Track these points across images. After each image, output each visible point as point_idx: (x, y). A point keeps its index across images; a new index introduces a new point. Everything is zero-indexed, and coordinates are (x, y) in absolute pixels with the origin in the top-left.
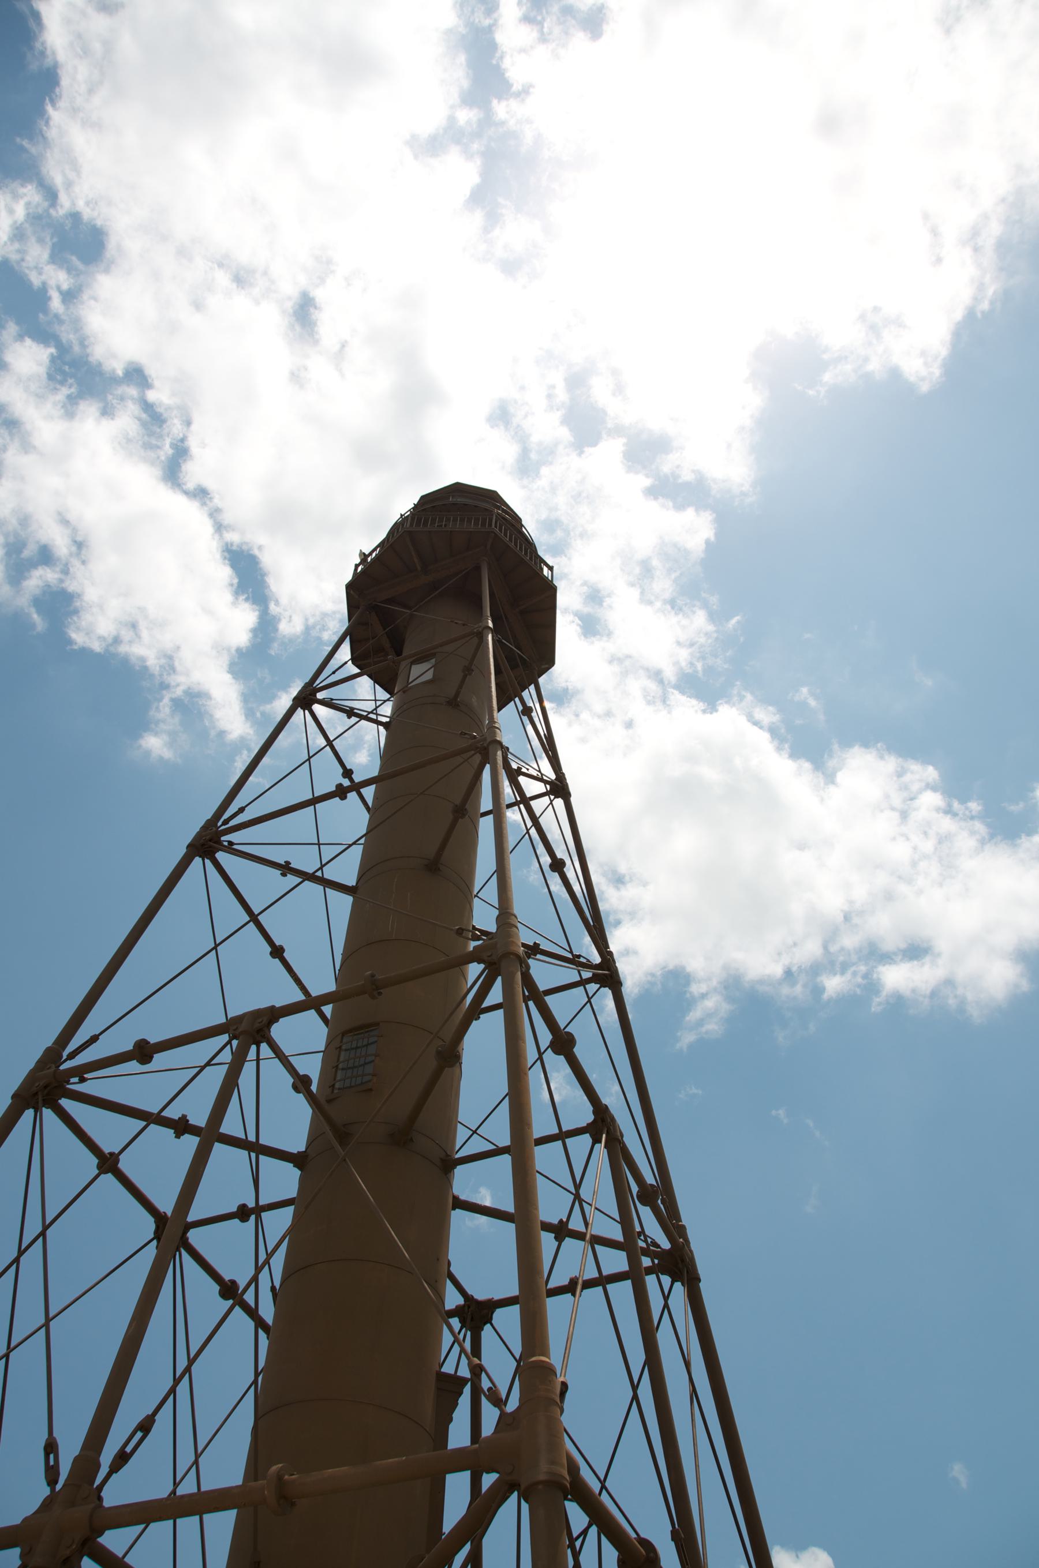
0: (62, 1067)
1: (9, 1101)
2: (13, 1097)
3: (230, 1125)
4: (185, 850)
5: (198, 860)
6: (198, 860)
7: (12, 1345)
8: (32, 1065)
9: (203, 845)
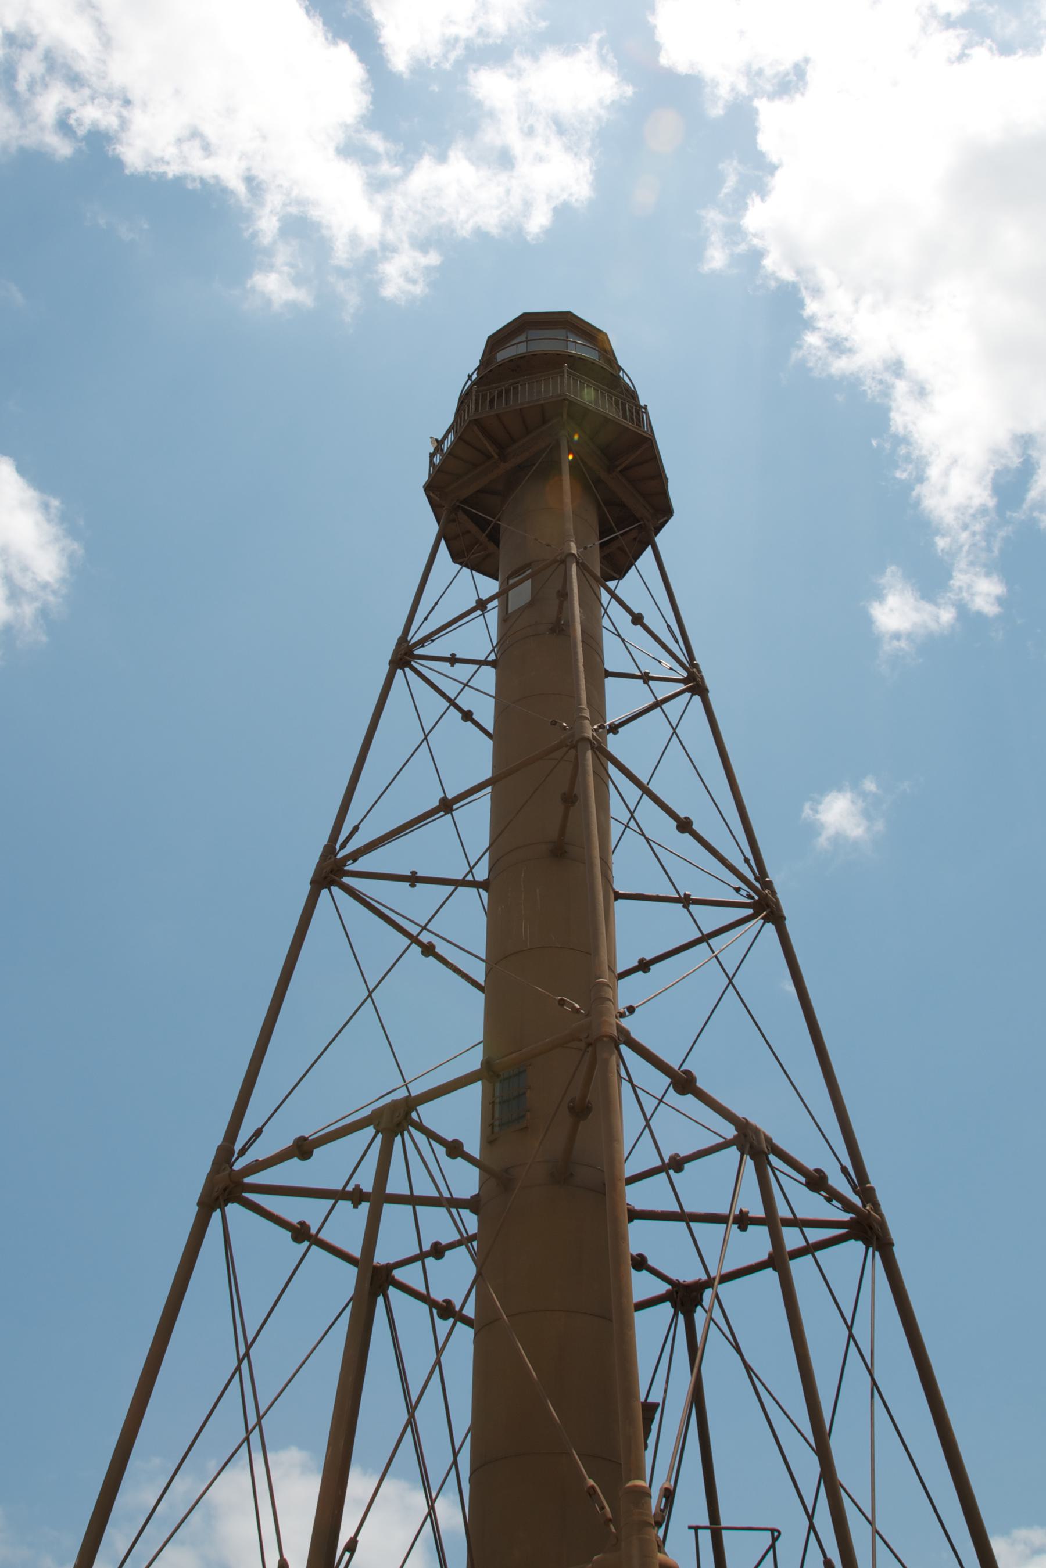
0: (339, 856)
1: (309, 887)
2: (311, 883)
3: (396, 1185)
4: (388, 667)
5: (399, 672)
6: (399, 672)
7: (261, 1413)
8: (317, 860)
9: (325, 878)
